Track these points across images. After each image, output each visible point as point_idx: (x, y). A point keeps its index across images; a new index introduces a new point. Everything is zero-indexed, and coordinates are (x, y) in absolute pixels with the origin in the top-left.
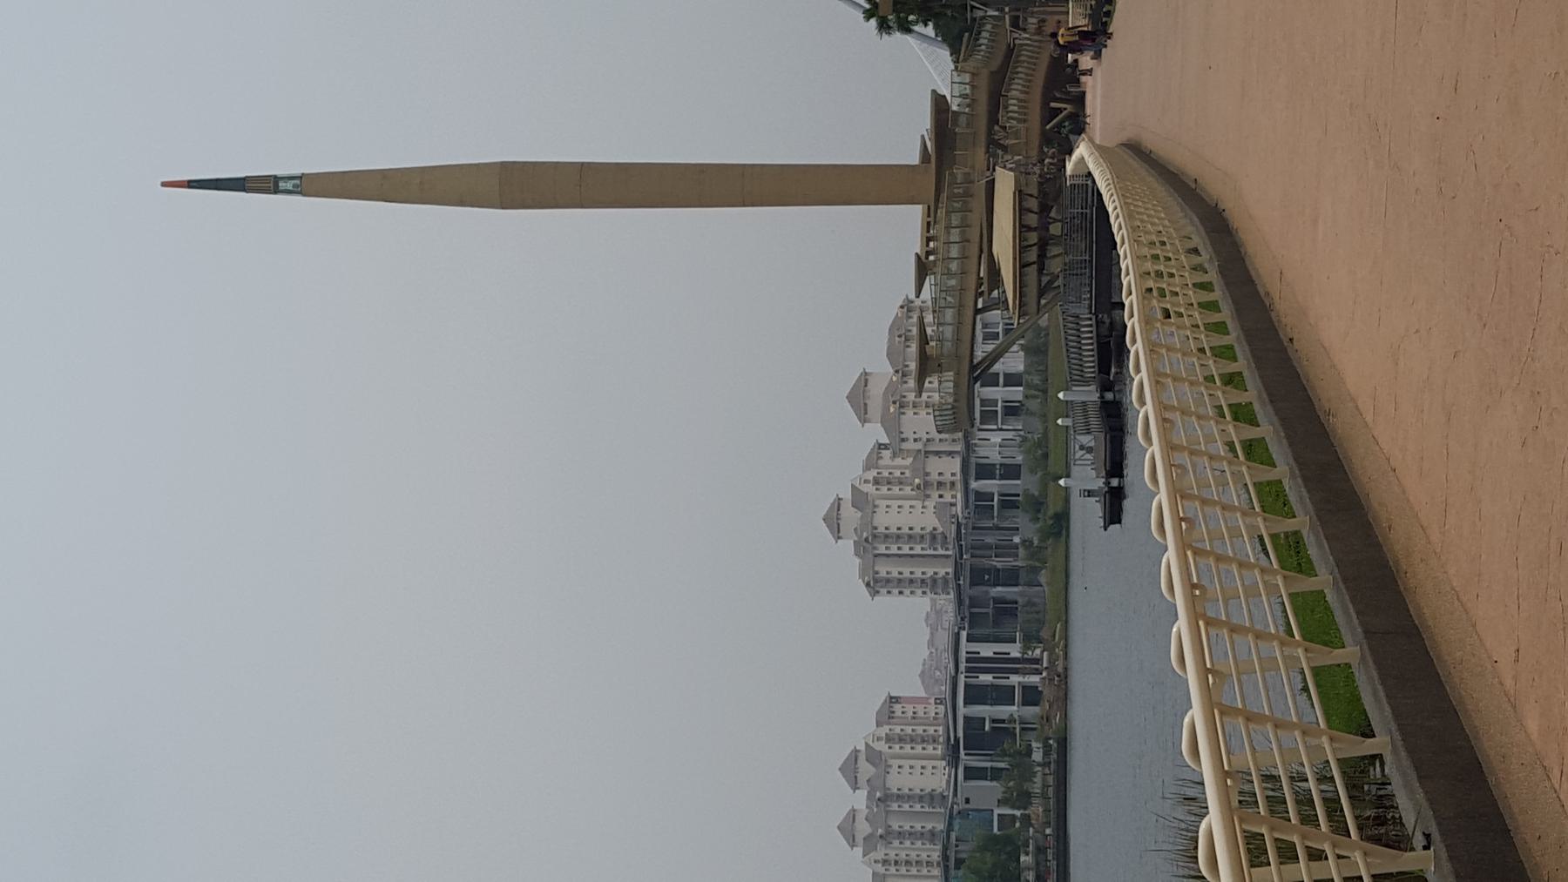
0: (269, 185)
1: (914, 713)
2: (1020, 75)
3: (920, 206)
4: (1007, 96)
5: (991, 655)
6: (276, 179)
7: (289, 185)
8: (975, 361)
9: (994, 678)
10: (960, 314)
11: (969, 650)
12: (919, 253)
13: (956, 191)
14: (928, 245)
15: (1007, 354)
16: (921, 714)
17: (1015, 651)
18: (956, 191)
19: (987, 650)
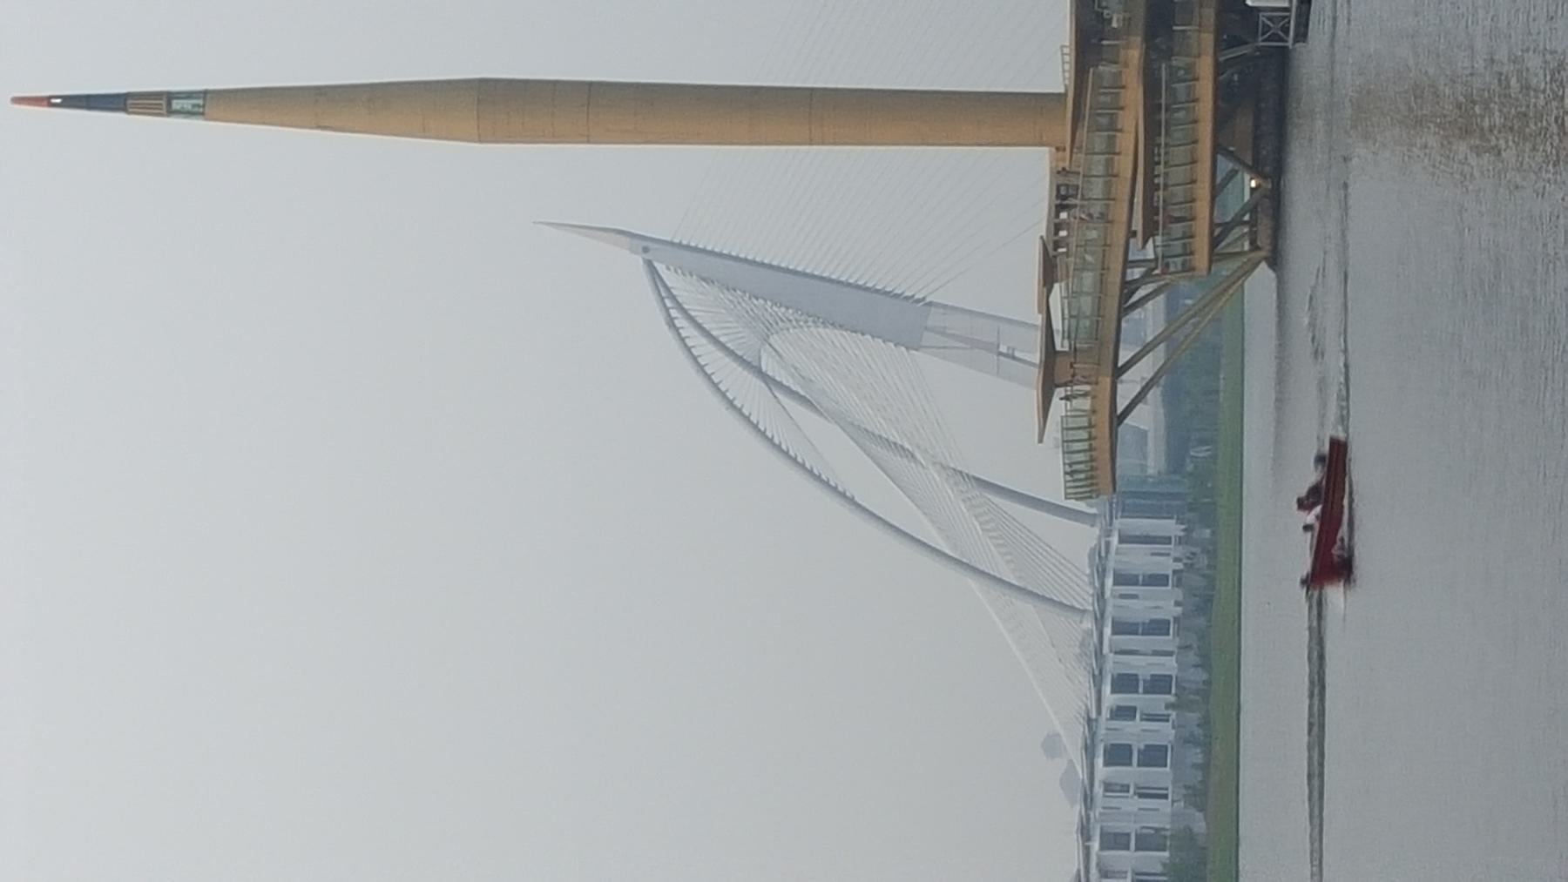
0: (161, 103)
3: (1046, 149)
6: (170, 96)
7: (187, 104)
8: (1120, 364)
10: (1102, 282)
12: (1045, 237)
13: (1102, 99)
14: (1057, 216)
18: (1102, 99)
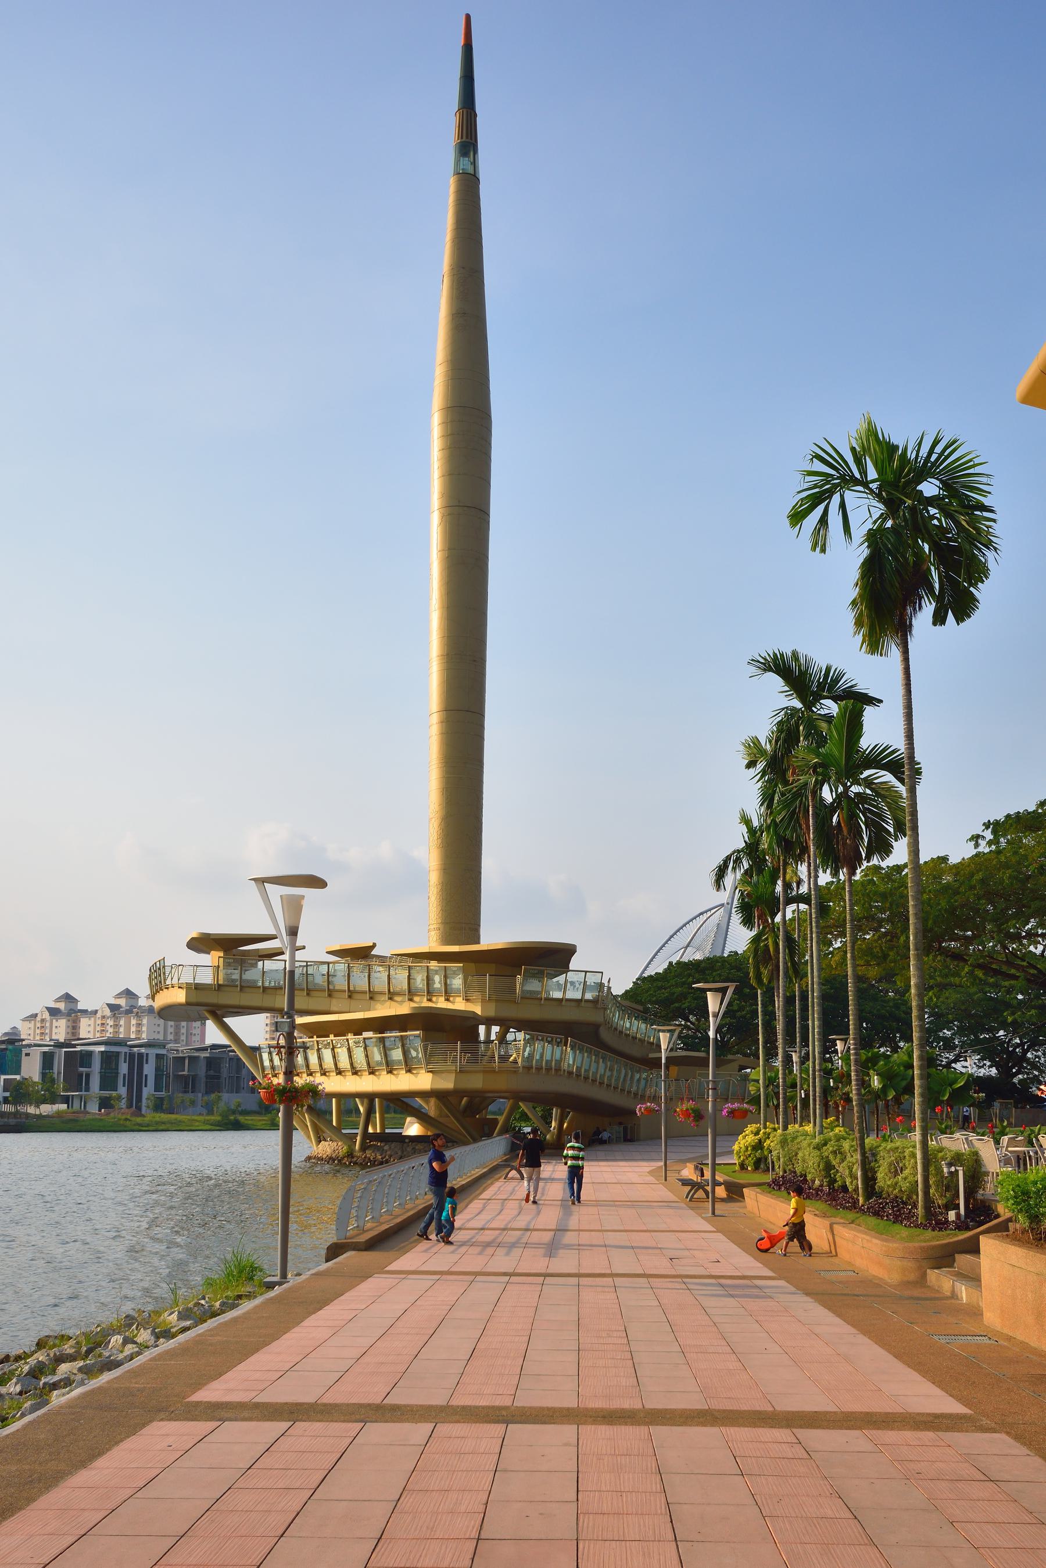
1: (195, 1035)
2: (594, 1065)
5: (145, 1073)
9: (125, 1075)
11: (150, 1056)
15: (476, 1201)
16: (194, 1038)
17: (148, 1091)
19: (149, 1069)
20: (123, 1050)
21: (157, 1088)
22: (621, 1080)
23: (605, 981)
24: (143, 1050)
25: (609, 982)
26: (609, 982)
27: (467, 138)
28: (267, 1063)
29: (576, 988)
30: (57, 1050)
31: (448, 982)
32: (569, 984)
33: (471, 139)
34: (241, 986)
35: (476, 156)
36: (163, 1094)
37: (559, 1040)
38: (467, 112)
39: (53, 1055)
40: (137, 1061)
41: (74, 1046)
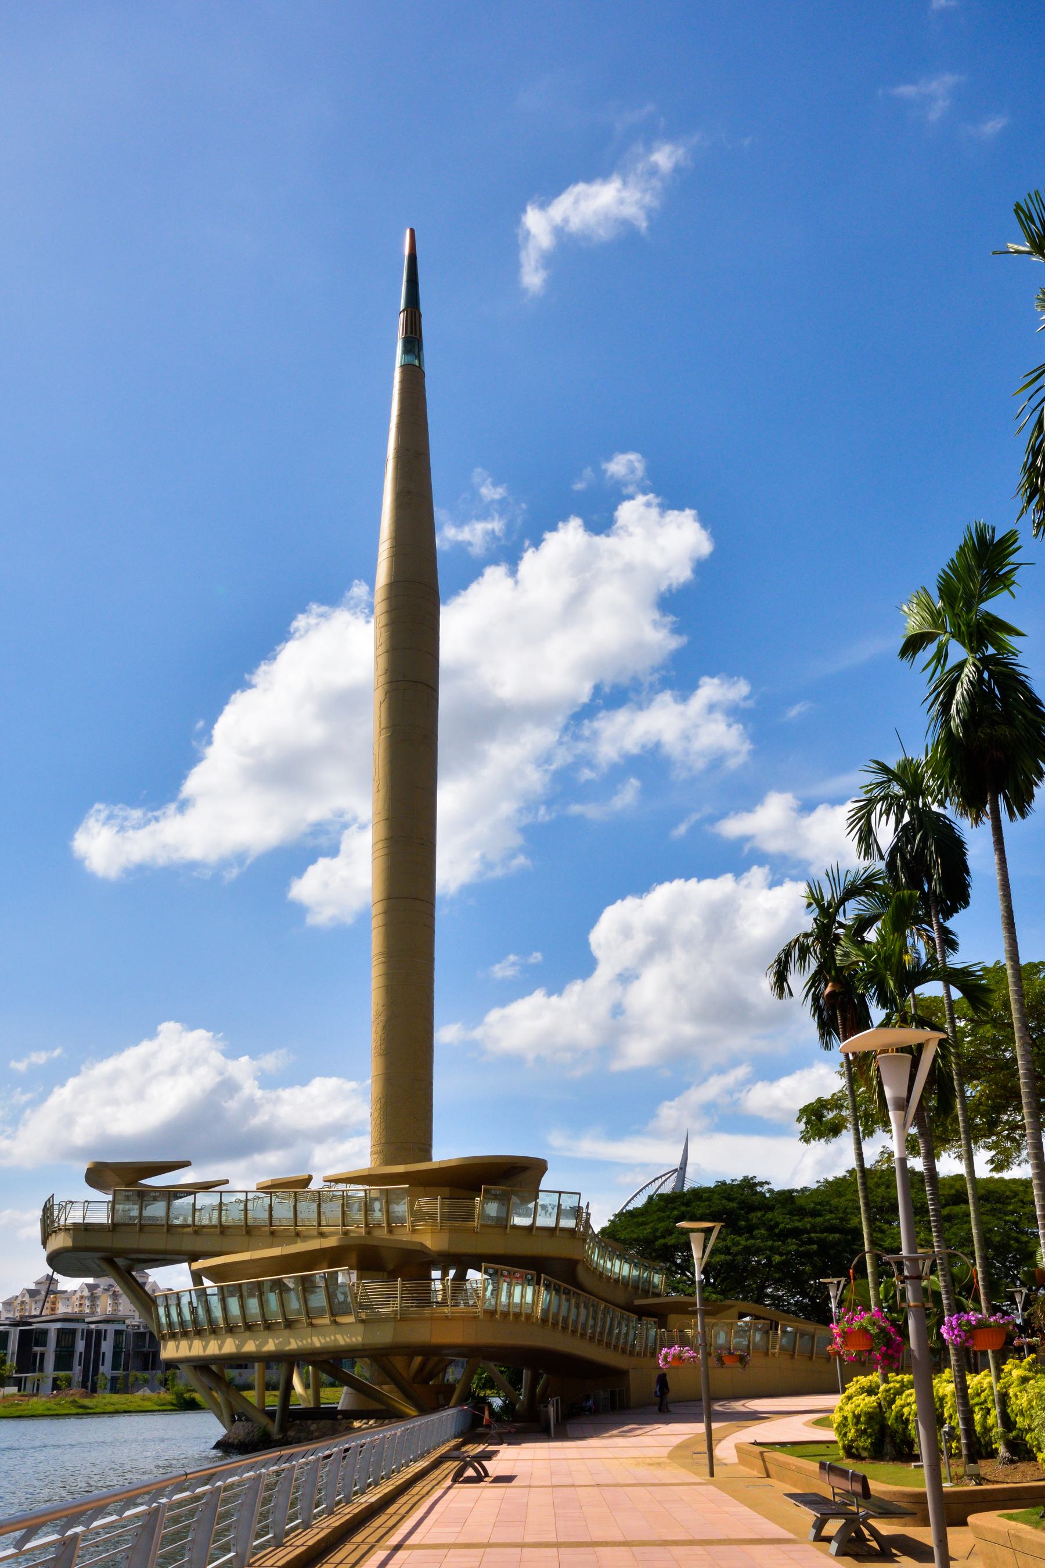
2: (573, 1310)
4: (538, 1283)
9: (81, 1353)
11: (108, 1332)
19: (107, 1346)
20: (80, 1326)
21: (115, 1366)
22: (607, 1331)
23: (583, 1205)
24: (102, 1326)
25: (587, 1207)
26: (587, 1207)
27: (412, 333)
28: (163, 1320)
29: (548, 1214)
30: (12, 1329)
31: (391, 1210)
32: (539, 1208)
33: (416, 335)
34: (141, 1225)
35: (421, 353)
36: (120, 1373)
37: (529, 1277)
38: (412, 311)
39: (8, 1336)
40: (94, 1338)
41: (30, 1324)
